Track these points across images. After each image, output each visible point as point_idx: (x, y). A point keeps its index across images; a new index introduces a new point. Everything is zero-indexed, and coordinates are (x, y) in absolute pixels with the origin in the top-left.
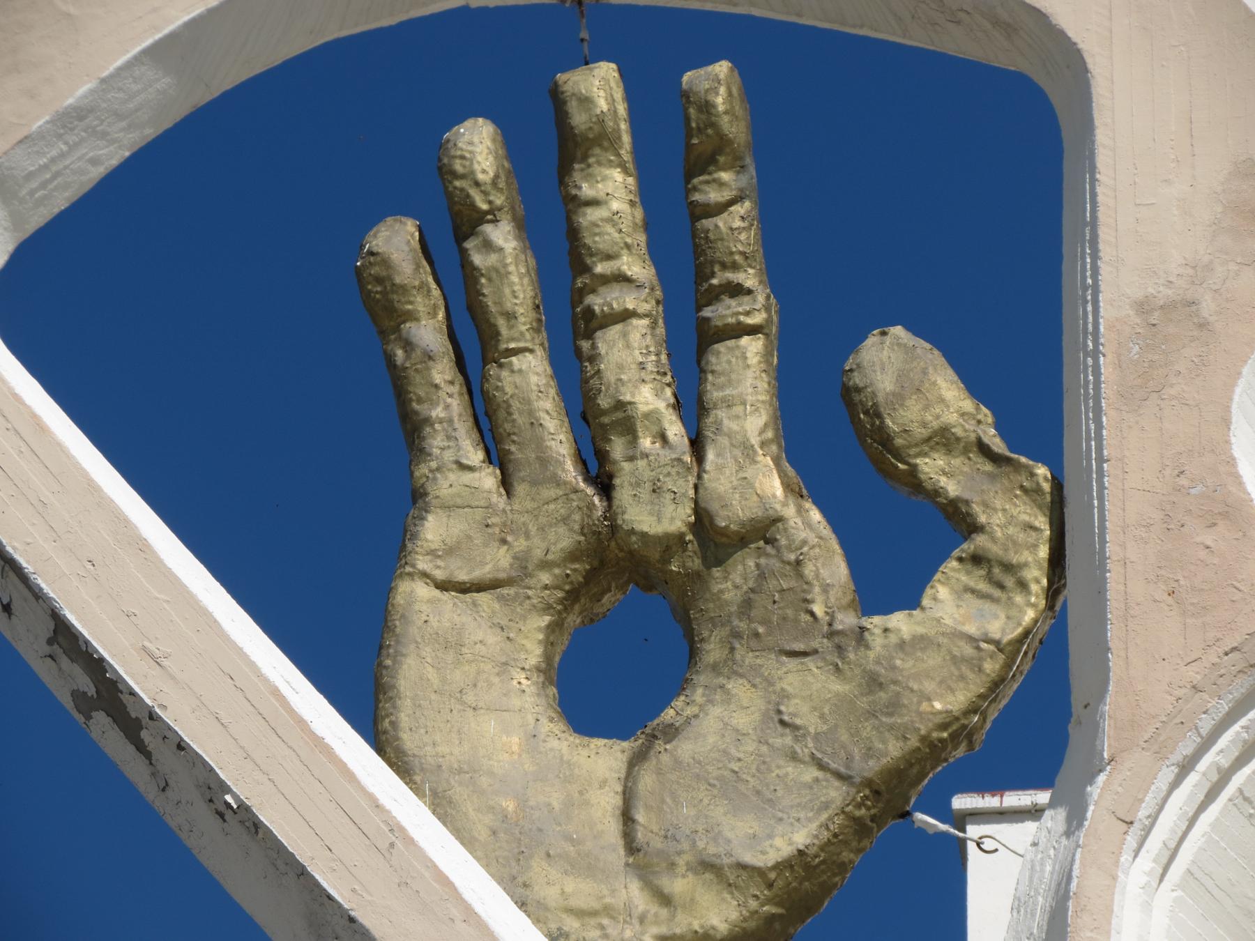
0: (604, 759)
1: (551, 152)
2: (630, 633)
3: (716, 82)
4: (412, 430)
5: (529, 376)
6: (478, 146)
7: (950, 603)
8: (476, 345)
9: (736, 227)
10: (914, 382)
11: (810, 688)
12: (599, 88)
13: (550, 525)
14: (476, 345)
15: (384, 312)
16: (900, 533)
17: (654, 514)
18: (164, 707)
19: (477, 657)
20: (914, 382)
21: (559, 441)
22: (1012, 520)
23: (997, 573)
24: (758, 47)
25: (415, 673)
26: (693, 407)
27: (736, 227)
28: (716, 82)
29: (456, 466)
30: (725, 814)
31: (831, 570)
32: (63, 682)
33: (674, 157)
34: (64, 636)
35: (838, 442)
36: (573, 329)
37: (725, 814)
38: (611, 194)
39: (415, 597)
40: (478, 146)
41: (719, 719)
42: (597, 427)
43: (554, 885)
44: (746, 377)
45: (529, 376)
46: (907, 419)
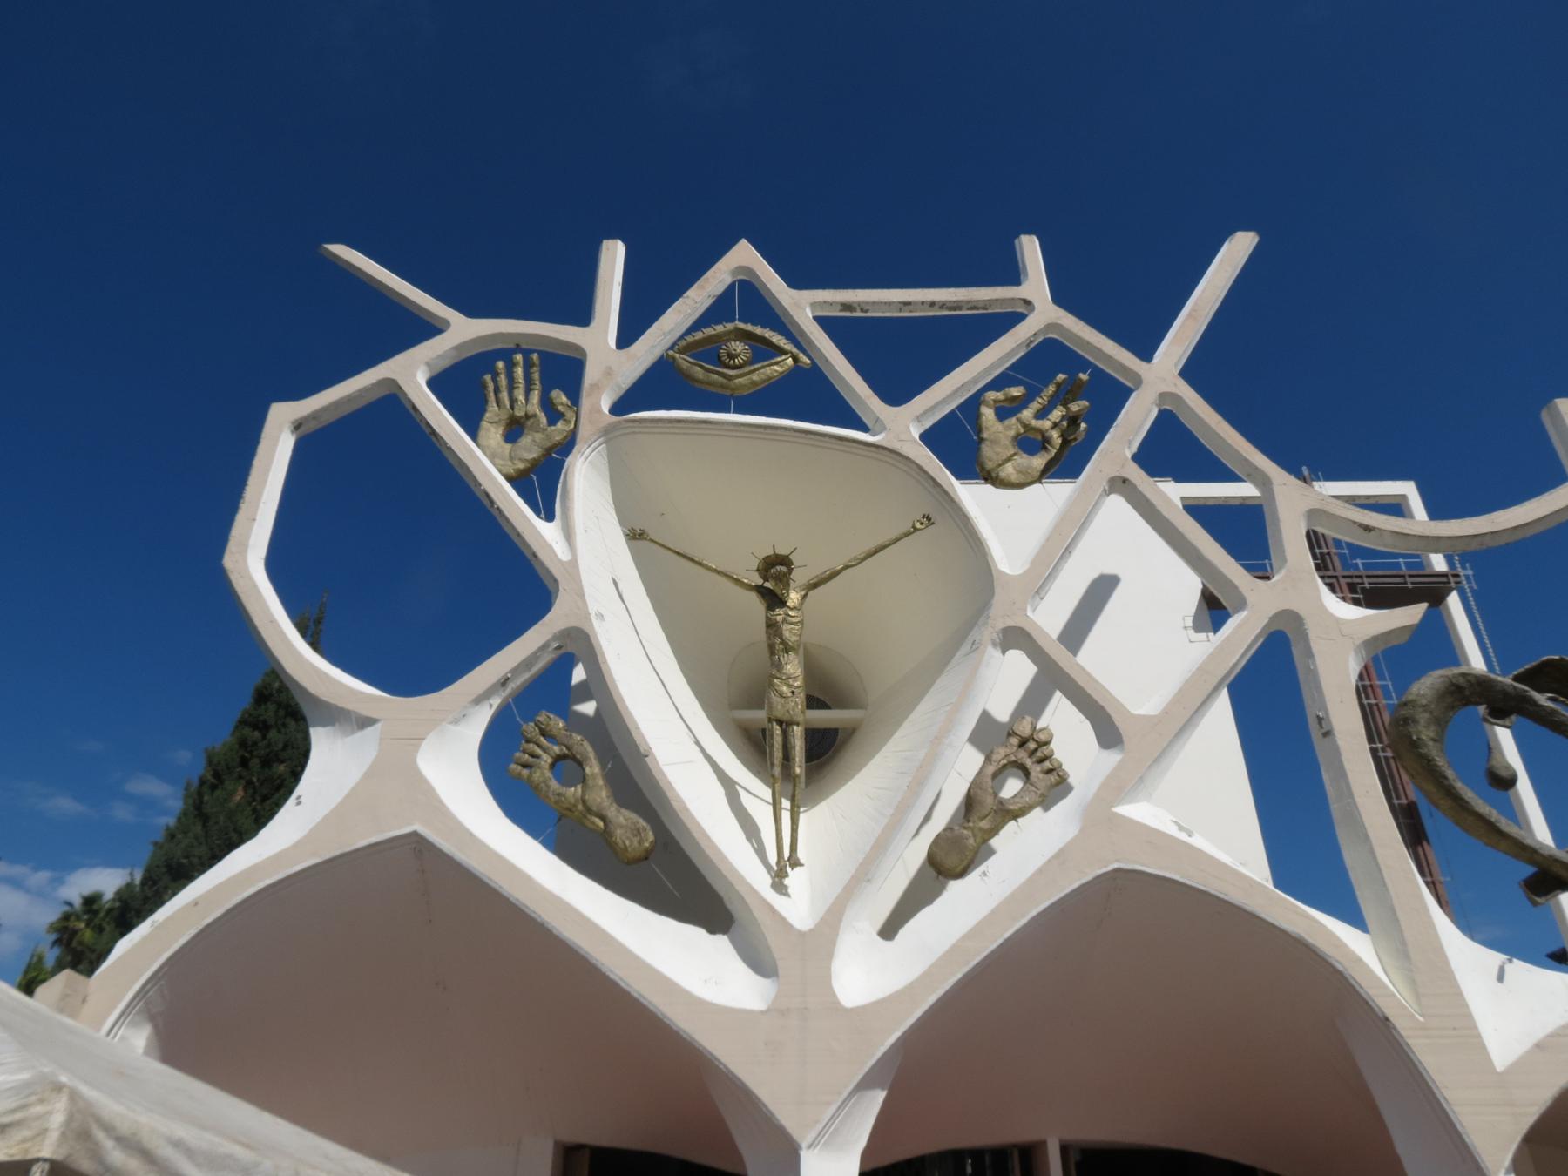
0: (508, 446)
1: (510, 365)
2: (514, 429)
3: (535, 356)
4: (486, 401)
5: (504, 395)
6: (500, 364)
7: (560, 425)
8: (497, 390)
9: (536, 376)
10: (560, 398)
11: (538, 436)
12: (519, 357)
13: (505, 416)
14: (497, 390)
15: (484, 386)
16: (554, 415)
17: (519, 413)
18: (600, 616)
19: (492, 433)
20: (560, 398)
21: (507, 403)
22: (570, 415)
23: (568, 422)
24: (539, 352)
25: (482, 433)
26: (527, 399)
27: (536, 376)
28: (535, 356)
29: (492, 408)
30: (994, 442)
31: (543, 419)
32: (427, 431)
33: (528, 365)
34: (428, 425)
35: (547, 405)
36: (511, 386)
37: (994, 442)
38: (519, 371)
39: (484, 424)
40: (500, 364)
41: (525, 440)
42: (513, 401)
43: (498, 461)
44: (535, 396)
45: (504, 395)
46: (556, 401)
